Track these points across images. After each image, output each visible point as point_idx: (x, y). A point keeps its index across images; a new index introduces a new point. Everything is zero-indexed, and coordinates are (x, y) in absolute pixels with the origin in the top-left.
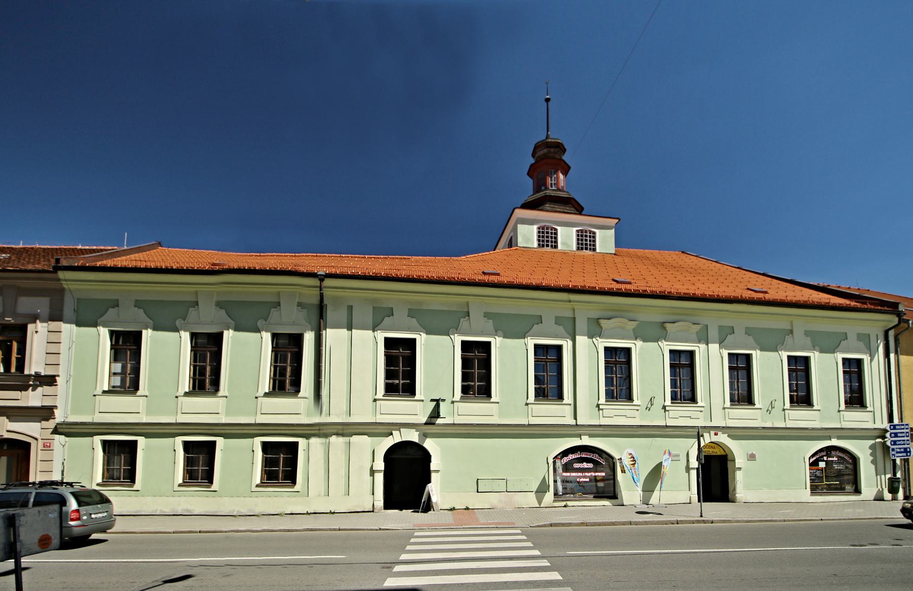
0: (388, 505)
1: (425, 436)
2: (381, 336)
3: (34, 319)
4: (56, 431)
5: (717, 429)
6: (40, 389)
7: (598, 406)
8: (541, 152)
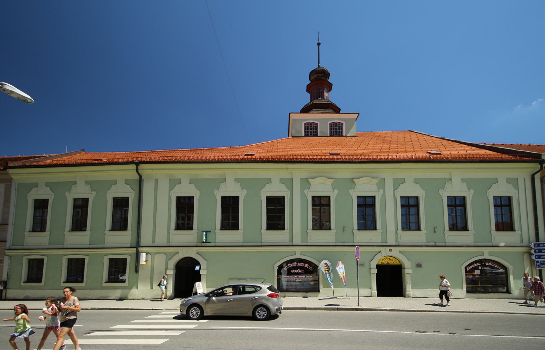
8: (313, 77)
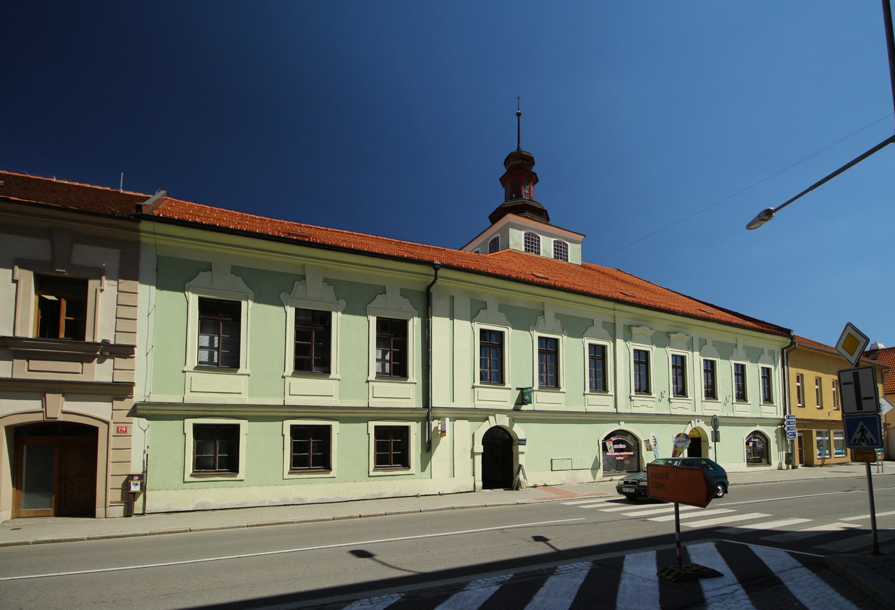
0: (485, 487)
1: (513, 421)
2: (478, 327)
3: (99, 274)
4: (134, 412)
6: (109, 362)
7: (630, 397)
8: (516, 162)
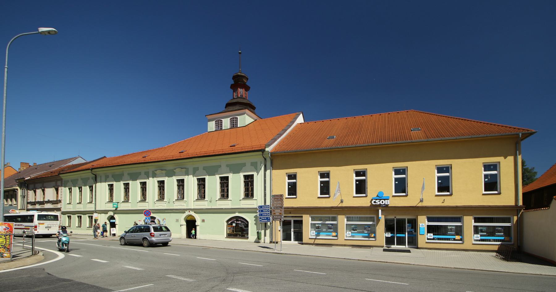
1: (115, 214)
5: (190, 210)
